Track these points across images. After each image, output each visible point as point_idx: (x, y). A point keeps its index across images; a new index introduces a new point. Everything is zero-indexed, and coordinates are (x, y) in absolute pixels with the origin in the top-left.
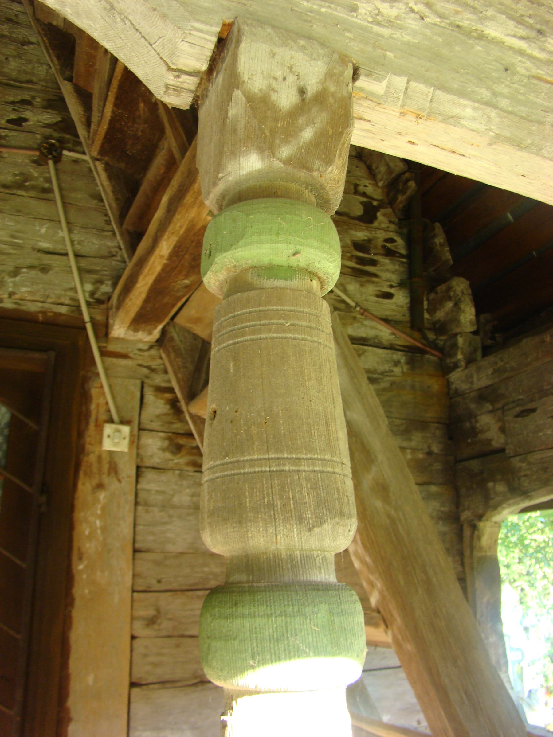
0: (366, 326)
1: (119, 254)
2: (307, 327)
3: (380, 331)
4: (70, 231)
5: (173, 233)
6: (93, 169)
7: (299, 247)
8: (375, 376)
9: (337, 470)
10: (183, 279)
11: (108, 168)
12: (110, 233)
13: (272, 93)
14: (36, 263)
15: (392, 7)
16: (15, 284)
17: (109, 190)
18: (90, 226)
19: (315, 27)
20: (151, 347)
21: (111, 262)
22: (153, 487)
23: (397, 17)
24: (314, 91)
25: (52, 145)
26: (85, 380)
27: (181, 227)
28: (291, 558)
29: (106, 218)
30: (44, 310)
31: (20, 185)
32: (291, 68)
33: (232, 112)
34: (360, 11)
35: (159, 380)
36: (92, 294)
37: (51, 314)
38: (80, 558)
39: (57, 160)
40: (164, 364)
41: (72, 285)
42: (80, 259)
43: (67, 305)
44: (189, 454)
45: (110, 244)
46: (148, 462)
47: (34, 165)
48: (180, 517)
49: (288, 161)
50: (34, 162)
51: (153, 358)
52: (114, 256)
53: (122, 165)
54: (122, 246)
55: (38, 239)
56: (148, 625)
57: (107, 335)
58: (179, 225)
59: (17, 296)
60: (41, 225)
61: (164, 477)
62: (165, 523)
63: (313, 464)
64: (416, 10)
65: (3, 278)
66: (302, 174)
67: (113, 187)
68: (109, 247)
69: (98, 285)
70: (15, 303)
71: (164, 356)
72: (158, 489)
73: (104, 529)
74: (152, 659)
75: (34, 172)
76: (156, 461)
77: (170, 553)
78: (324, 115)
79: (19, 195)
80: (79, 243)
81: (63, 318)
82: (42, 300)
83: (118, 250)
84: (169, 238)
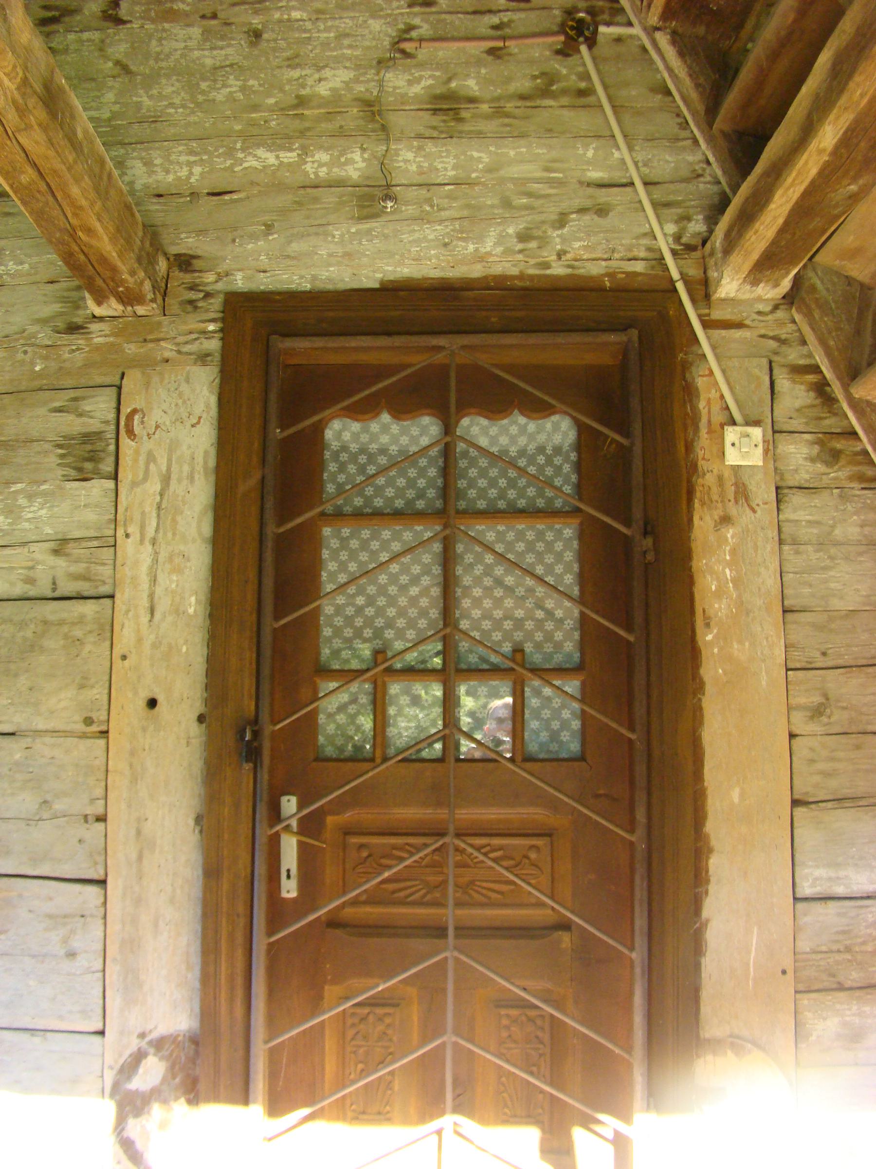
1: (708, 171)
4: (631, 149)
5: (846, 109)
6: (649, 46)
10: (849, 185)
11: (676, 39)
12: (689, 142)
14: (588, 203)
16: (564, 239)
18: (657, 135)
20: (776, 307)
21: (697, 186)
22: (802, 516)
25: (581, 21)
26: (686, 366)
27: (862, 96)
29: (680, 120)
30: (611, 270)
31: (545, 92)
35: (794, 355)
36: (677, 238)
38: (708, 625)
39: (591, 42)
40: (799, 330)
42: (651, 187)
43: (642, 259)
45: (690, 158)
47: (560, 57)
48: (847, 559)
50: (558, 52)
51: (780, 324)
52: (699, 176)
53: (701, 30)
54: (712, 159)
55: (585, 167)
56: (812, 718)
57: (707, 296)
60: (586, 147)
61: (817, 501)
62: (825, 569)
65: (545, 232)
67: (690, 68)
68: (691, 164)
69: (685, 222)
70: (569, 266)
71: (797, 317)
74: (821, 766)
75: (560, 67)
79: (545, 107)
80: (645, 165)
81: (640, 278)
82: (605, 256)
83: (705, 166)
84: (837, 118)
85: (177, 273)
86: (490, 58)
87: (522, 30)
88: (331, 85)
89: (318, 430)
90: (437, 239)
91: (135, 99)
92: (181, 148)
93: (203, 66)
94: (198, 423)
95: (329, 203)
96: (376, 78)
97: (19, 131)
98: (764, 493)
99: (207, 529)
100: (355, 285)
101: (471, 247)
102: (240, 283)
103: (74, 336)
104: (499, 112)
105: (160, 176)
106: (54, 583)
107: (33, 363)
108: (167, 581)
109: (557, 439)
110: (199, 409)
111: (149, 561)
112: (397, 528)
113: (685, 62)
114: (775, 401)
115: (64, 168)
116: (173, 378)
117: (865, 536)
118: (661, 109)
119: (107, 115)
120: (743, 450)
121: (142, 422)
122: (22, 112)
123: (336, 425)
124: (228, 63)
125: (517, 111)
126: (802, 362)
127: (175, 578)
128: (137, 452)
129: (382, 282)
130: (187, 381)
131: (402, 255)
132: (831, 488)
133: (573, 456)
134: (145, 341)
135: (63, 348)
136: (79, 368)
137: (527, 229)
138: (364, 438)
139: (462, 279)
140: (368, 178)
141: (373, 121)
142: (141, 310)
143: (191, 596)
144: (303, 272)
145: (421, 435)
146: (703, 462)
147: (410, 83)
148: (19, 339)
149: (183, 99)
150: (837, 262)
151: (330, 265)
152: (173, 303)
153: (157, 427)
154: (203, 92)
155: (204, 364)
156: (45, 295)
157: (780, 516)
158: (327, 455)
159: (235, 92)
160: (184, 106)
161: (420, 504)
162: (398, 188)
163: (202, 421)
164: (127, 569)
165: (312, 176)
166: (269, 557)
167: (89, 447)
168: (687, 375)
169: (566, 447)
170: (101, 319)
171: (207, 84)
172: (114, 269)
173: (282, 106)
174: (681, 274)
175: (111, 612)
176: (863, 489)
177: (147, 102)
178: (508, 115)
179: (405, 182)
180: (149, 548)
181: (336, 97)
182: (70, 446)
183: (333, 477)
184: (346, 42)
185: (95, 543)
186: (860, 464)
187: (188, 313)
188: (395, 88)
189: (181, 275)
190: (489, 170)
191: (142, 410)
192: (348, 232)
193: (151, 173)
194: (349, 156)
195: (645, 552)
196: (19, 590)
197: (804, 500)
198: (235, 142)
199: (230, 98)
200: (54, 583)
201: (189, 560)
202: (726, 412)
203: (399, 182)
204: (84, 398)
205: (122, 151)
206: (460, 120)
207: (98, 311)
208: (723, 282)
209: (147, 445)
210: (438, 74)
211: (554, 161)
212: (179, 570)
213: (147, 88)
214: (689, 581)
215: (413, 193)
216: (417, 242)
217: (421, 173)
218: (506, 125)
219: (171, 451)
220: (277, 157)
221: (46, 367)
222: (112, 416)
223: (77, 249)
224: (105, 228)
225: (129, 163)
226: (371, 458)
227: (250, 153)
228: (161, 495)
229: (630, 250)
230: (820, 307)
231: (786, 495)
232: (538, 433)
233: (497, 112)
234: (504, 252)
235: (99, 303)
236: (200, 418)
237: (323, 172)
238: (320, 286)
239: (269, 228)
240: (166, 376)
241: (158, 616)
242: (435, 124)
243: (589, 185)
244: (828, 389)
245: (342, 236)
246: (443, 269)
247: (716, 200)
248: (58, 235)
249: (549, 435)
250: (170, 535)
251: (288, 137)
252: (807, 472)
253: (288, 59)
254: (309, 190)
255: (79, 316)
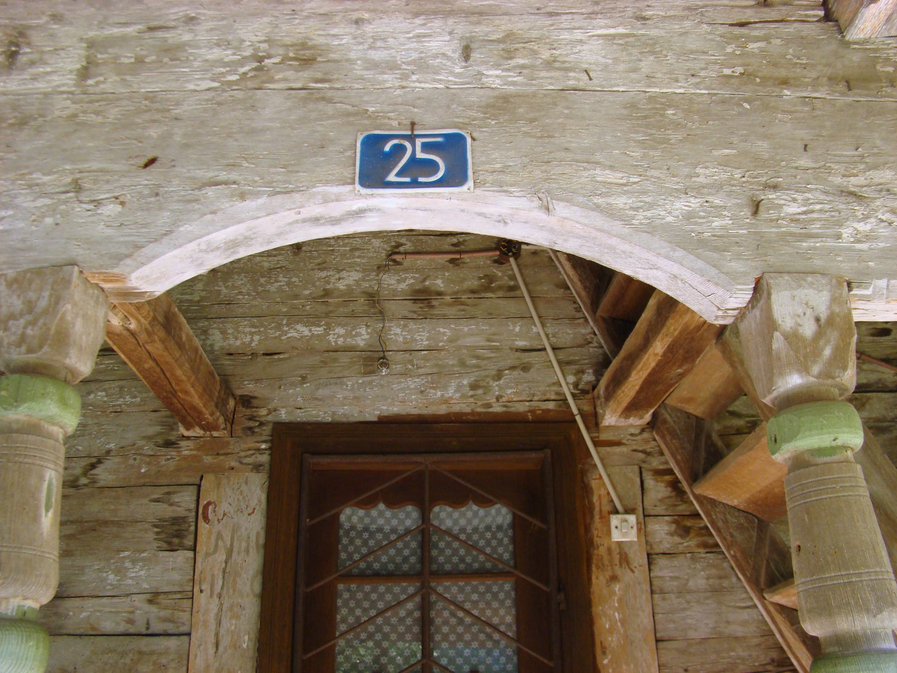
0: (865, 371)
1: (595, 339)
2: (850, 486)
3: (883, 373)
4: (543, 325)
7: (836, 435)
8: (885, 424)
9: (885, 577)
12: (582, 320)
13: (799, 328)
14: (517, 363)
15: (866, 224)
16: (501, 388)
17: (576, 279)
18: (561, 316)
19: (815, 261)
20: (643, 430)
22: (666, 573)
23: (872, 231)
24: (825, 317)
26: (584, 473)
27: (675, 330)
28: (865, 634)
29: (576, 306)
30: (533, 408)
31: (487, 288)
32: (807, 304)
33: (775, 346)
34: (843, 236)
35: (656, 463)
36: (576, 385)
37: (540, 412)
38: (604, 653)
40: (659, 446)
41: (555, 380)
43: (553, 400)
44: (699, 535)
45: (583, 331)
46: (658, 549)
47: (496, 265)
48: (698, 602)
49: (818, 376)
50: (496, 261)
51: (646, 441)
52: (590, 343)
54: (597, 333)
55: (514, 338)
57: (597, 424)
58: (672, 328)
59: (504, 399)
60: (515, 325)
61: (676, 562)
62: (684, 609)
63: (870, 576)
64: (884, 219)
65: (488, 383)
66: (830, 381)
67: (580, 276)
68: (584, 335)
69: (581, 375)
70: (505, 406)
71: (657, 438)
72: (671, 574)
73: (623, 621)
76: (665, 546)
77: (693, 639)
78: (836, 333)
80: (554, 336)
81: (552, 413)
82: (528, 399)
84: (663, 339)
85: (241, 408)
86: (451, 265)
87: (472, 247)
88: (346, 282)
89: (336, 517)
90: (416, 388)
91: (216, 288)
92: (246, 323)
93: (262, 267)
94: (253, 512)
95: (345, 363)
96: (376, 278)
97: (147, 343)
98: (639, 558)
99: (257, 588)
100: (361, 419)
101: (439, 393)
102: (283, 416)
103: (170, 449)
104: (457, 301)
105: (232, 341)
106: (148, 624)
107: (140, 467)
108: (228, 624)
109: (499, 520)
110: (254, 503)
111: (216, 609)
112: (390, 584)
113: (577, 272)
114: (645, 495)
115: (173, 361)
116: (236, 481)
117: (710, 585)
118: (563, 298)
119: (197, 298)
120: (624, 531)
121: (214, 511)
122: (149, 334)
123: (348, 511)
124: (279, 266)
125: (469, 300)
126: (661, 467)
127: (234, 622)
128: (210, 532)
129: (379, 417)
130: (246, 483)
131: (393, 399)
132: (685, 553)
133: (510, 532)
134: (218, 454)
135: (161, 457)
136: (172, 471)
137: (475, 381)
138: (367, 520)
139: (433, 415)
140: (370, 346)
141: (374, 307)
142: (215, 434)
143: (245, 635)
144: (326, 409)
145: (406, 518)
146: (597, 539)
147: (399, 282)
148: (130, 450)
149: (248, 290)
150: (679, 404)
151: (345, 405)
152: (238, 428)
153: (224, 515)
154: (262, 285)
155: (258, 471)
156: (151, 420)
157: (652, 575)
158: (341, 532)
159: (283, 285)
160: (249, 294)
161: (405, 567)
162: (391, 353)
163: (256, 511)
164: (201, 615)
165: (333, 344)
166: (300, 608)
167: (176, 527)
168: (585, 479)
169: (505, 526)
170: (188, 438)
171: (264, 279)
172: (200, 413)
173: (315, 296)
174: (579, 410)
175: (188, 645)
176: (707, 553)
177: (224, 291)
178: (463, 304)
179: (395, 349)
180: (217, 600)
181: (350, 290)
182: (162, 526)
183: (346, 547)
184: (357, 253)
185: (179, 596)
186: (703, 535)
187: (247, 436)
188: (389, 285)
189: (244, 409)
190: (451, 341)
191: (214, 503)
192: (357, 383)
193: (225, 339)
194: (358, 330)
195: (559, 603)
196: (122, 628)
197: (668, 563)
198: (282, 320)
199: (280, 290)
200: (148, 624)
201: (244, 609)
202: (612, 503)
203: (391, 349)
204: (174, 493)
205: (206, 323)
206: (432, 307)
207: (186, 433)
208: (606, 417)
209: (217, 527)
210: (417, 275)
211: (494, 334)
212: (236, 617)
213: (225, 281)
214: (589, 622)
215: (400, 356)
216: (403, 389)
217: (406, 343)
218: (463, 310)
219: (234, 532)
220: (310, 331)
221: (149, 470)
222: (193, 506)
223: (176, 401)
224: (196, 391)
225: (211, 331)
226: (372, 535)
227: (292, 327)
228: (226, 563)
229: (545, 395)
230: (670, 434)
231: (654, 559)
232: (486, 516)
233: (456, 302)
234: (461, 397)
235: (188, 429)
236: (254, 509)
237: (340, 341)
238: (338, 419)
239: (304, 379)
240: (232, 479)
241: (221, 649)
242: (415, 309)
243: (517, 350)
244: (679, 485)
245: (353, 385)
246: (420, 408)
247: (601, 358)
248: (165, 394)
249: (494, 518)
250: (231, 591)
251: (317, 317)
252: (668, 543)
253: (319, 264)
254: (331, 353)
255: (173, 435)
